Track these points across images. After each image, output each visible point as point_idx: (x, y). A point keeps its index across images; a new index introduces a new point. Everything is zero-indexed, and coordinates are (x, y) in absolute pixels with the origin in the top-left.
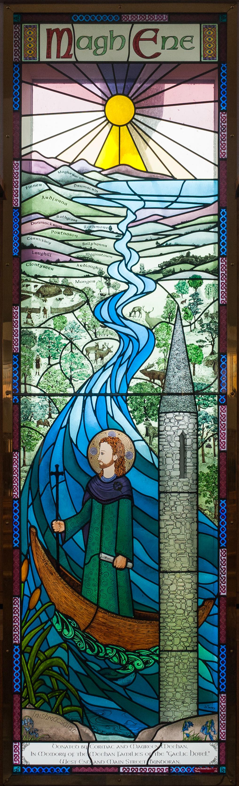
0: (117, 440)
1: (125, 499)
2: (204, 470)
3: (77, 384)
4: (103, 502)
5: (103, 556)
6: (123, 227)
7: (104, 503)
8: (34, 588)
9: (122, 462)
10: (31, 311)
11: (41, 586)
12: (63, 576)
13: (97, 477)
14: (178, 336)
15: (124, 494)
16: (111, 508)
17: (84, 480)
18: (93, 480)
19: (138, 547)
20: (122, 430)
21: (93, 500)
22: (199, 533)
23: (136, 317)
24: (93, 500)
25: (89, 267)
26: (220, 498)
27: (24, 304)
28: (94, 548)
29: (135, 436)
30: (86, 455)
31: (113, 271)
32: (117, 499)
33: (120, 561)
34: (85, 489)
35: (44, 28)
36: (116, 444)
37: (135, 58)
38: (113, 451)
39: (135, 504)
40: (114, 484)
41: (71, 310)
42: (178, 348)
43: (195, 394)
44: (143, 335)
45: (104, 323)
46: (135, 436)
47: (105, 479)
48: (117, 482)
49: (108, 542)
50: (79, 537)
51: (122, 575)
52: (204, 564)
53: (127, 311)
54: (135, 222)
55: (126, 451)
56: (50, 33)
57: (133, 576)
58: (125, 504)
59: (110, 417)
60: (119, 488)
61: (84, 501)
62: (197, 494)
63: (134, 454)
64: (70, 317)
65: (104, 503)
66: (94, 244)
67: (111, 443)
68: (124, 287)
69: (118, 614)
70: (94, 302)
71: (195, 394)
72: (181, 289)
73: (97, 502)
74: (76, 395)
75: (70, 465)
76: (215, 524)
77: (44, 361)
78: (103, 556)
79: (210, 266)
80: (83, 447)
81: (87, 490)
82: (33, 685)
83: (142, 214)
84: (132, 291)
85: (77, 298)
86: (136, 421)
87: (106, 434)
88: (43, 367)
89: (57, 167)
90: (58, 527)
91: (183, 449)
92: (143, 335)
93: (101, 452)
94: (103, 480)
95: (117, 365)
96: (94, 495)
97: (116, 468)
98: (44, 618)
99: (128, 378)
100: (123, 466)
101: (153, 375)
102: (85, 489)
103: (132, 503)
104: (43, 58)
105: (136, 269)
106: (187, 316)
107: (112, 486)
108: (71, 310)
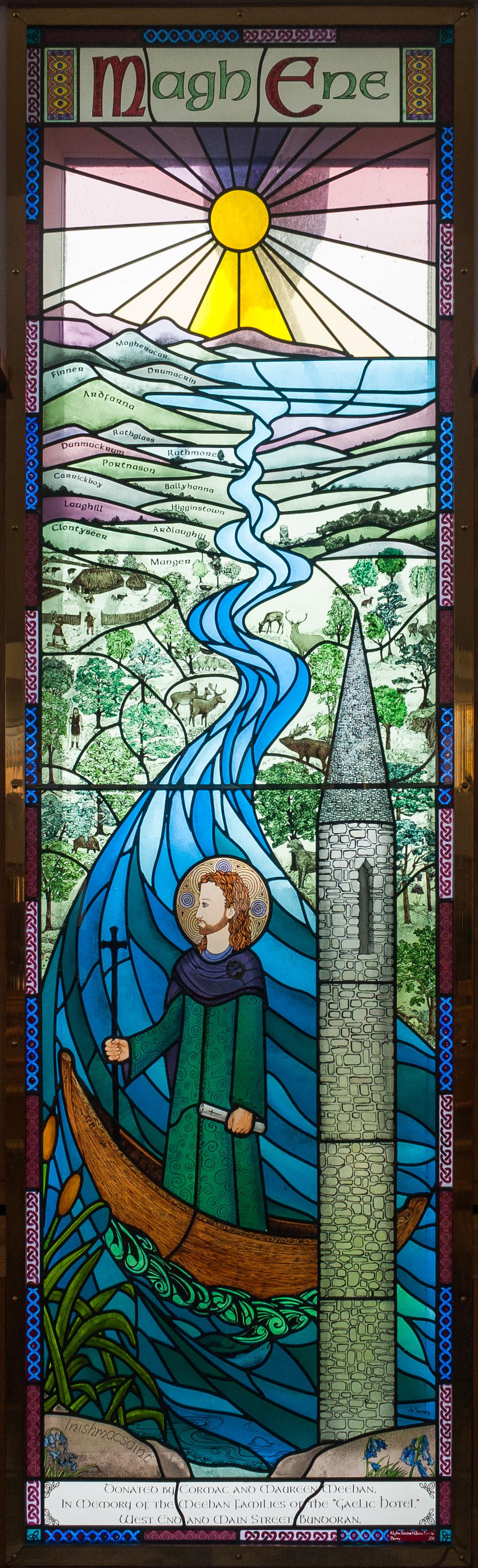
0: (234, 877)
1: (250, 996)
2: (408, 937)
3: (155, 767)
4: (206, 1002)
5: (206, 1109)
6: (246, 453)
7: (208, 1003)
8: (69, 1173)
9: (243, 922)
10: (62, 620)
11: (82, 1170)
12: (126, 1148)
13: (193, 951)
14: (357, 670)
15: (248, 985)
16: (222, 1013)
17: (169, 958)
18: (186, 957)
19: (275, 1091)
20: (245, 858)
21: (187, 997)
22: (397, 1063)
23: (273, 633)
24: (187, 997)
25: (178, 533)
26: (439, 994)
27: (48, 606)
28: (188, 1093)
29: (270, 869)
30: (172, 909)
31: (227, 541)
32: (235, 996)
33: (241, 1120)
34: (170, 976)
35: (88, 55)
36: (233, 885)
37: (269, 115)
38: (227, 900)
39: (270, 1005)
40: (227, 967)
41: (143, 619)
42: (357, 695)
43: (389, 785)
44: (286, 669)
45: (208, 645)
46: (270, 869)
47: (211, 956)
48: (235, 962)
49: (216, 1081)
50: (158, 1071)
51: (243, 1147)
52: (409, 1125)
53: (253, 620)
54: (271, 444)
55: (252, 901)
56: (99, 65)
57: (267, 1148)
58: (250, 1006)
59: (220, 831)
60: (238, 973)
61: (169, 999)
62: (394, 985)
63: (268, 906)
64: (139, 633)
65: (208, 1003)
66: (189, 488)
67: (222, 883)
68: (247, 572)
69: (236, 1225)
70: (188, 602)
71: (389, 785)
72: (361, 577)
73: (193, 1002)
74: (151, 788)
75: (140, 927)
76: (430, 1046)
77: (88, 720)
78: (206, 1109)
79: (421, 530)
80: (165, 892)
81: (174, 977)
82: (66, 1366)
83: (283, 428)
84: (265, 580)
85: (154, 595)
86: (272, 839)
87: (213, 866)
88: (86, 733)
89: (114, 333)
90: (117, 1050)
91: (366, 896)
92: (286, 669)
93: (201, 902)
94: (206, 958)
95: (234, 728)
96: (187, 988)
97: (231, 933)
98: (88, 1232)
99: (256, 754)
100: (246, 930)
101: (305, 749)
102: (170, 976)
103: (263, 1004)
104: (87, 115)
105: (273, 537)
106: (374, 630)
107: (225, 969)
108: (143, 619)
